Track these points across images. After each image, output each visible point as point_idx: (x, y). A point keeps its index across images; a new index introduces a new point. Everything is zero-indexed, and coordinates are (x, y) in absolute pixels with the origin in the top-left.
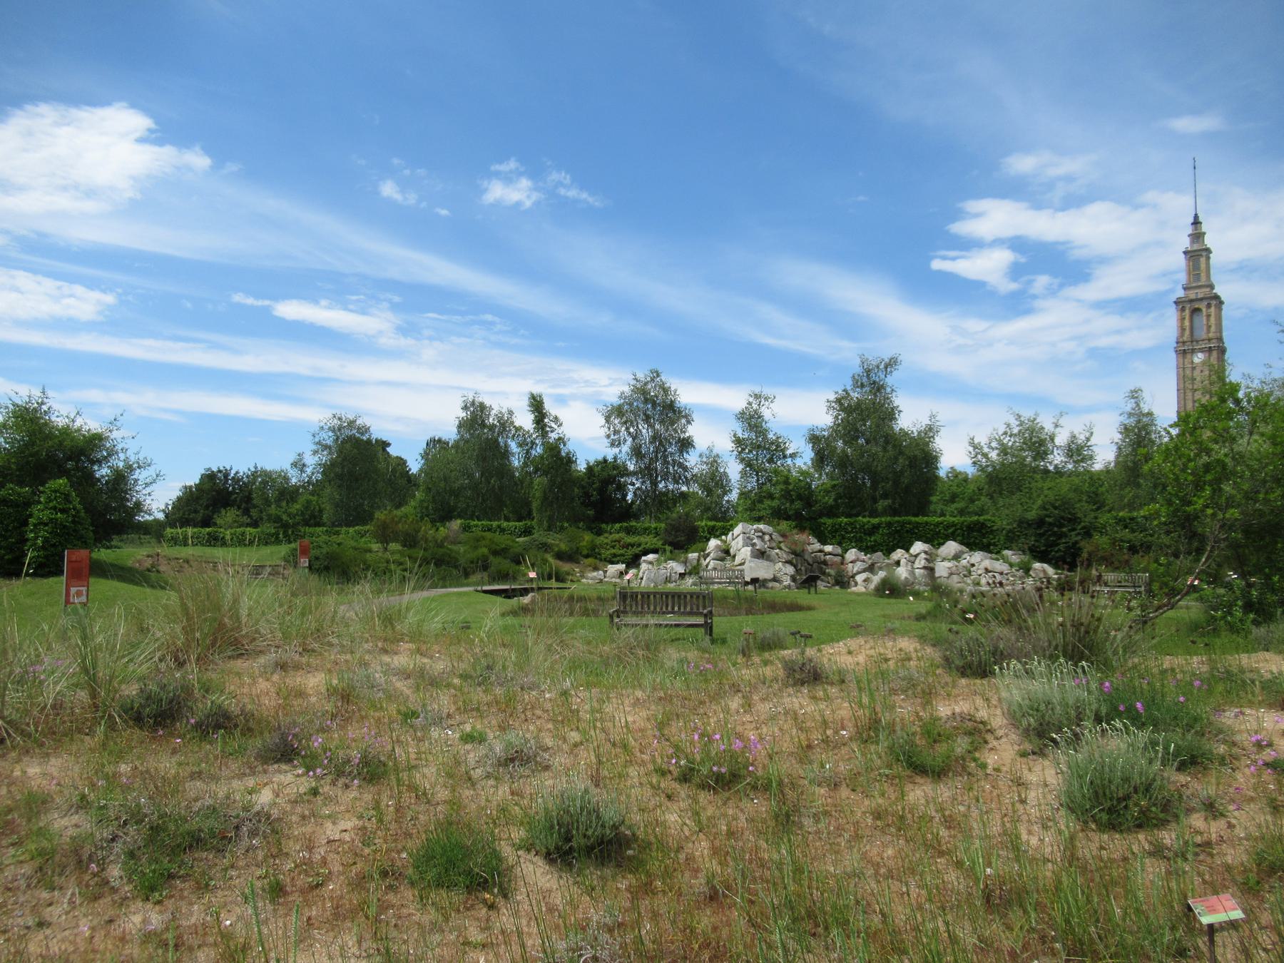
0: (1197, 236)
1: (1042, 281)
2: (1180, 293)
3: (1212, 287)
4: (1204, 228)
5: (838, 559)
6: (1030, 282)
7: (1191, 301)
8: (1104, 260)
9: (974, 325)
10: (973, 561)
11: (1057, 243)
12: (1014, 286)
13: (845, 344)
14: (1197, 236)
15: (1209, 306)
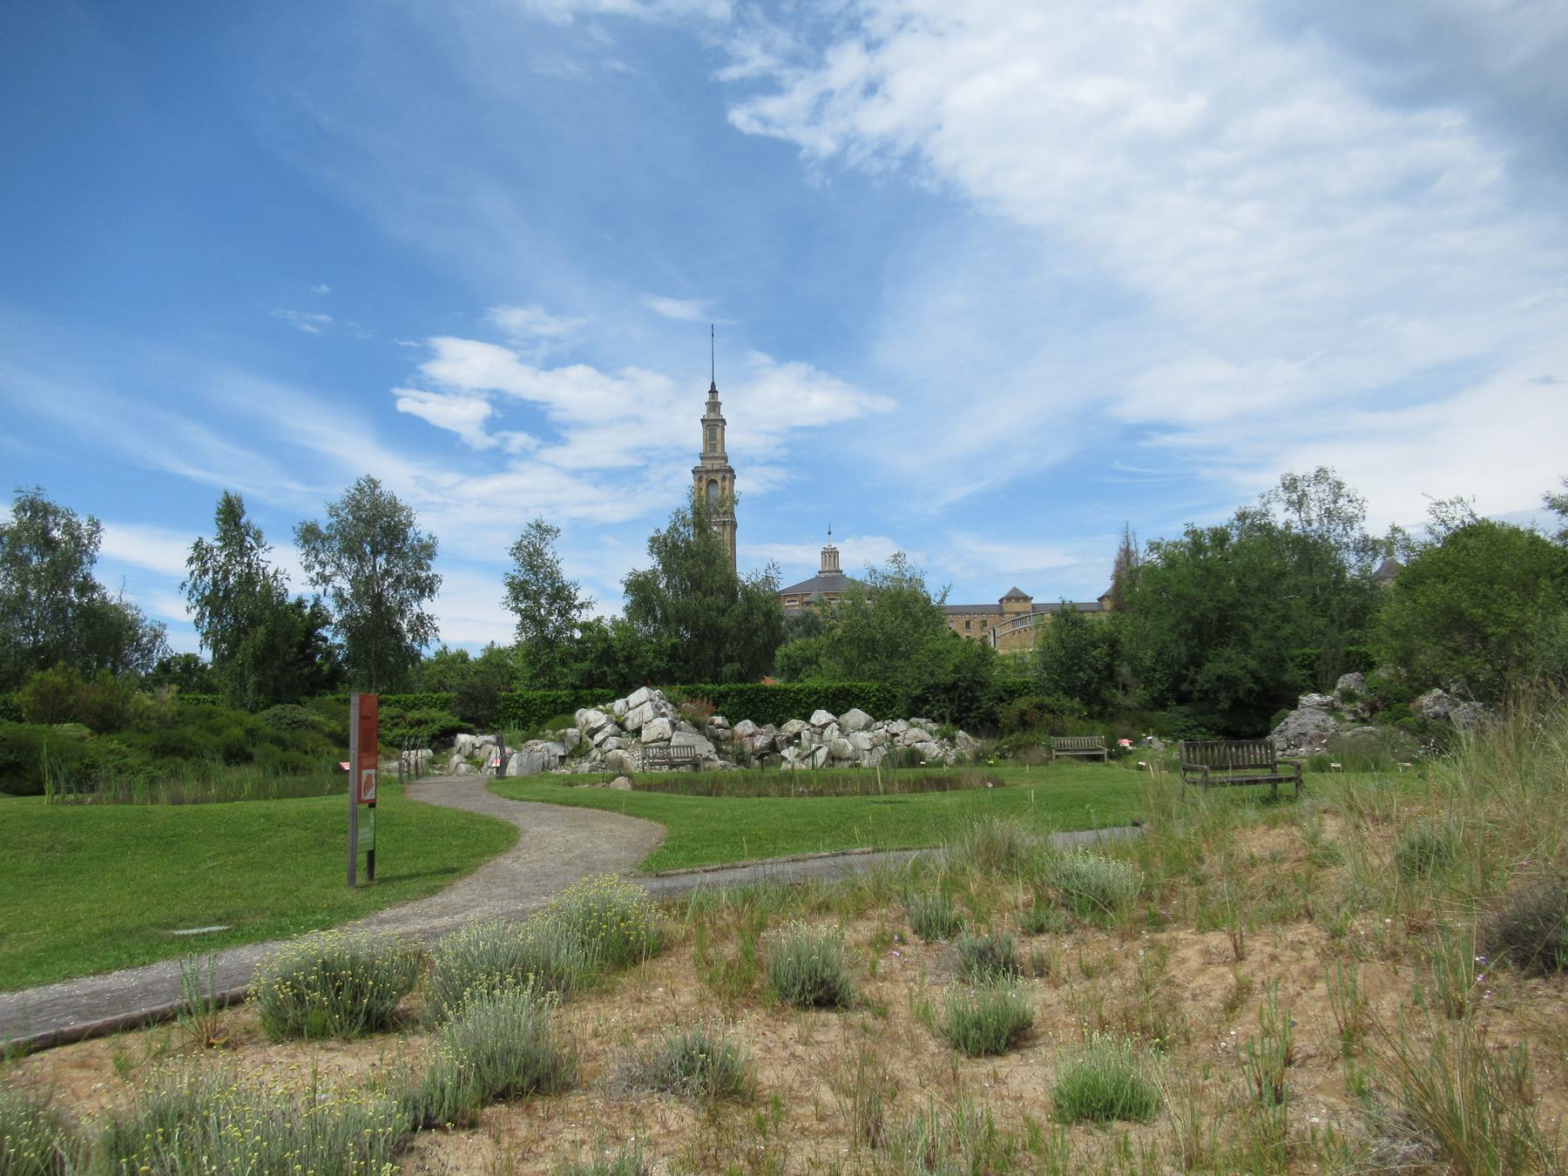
0: (714, 406)
1: (519, 440)
2: (698, 463)
3: (726, 459)
4: (720, 398)
5: (728, 733)
6: (506, 440)
7: (708, 472)
8: (582, 426)
9: (449, 478)
10: (894, 730)
11: (535, 403)
12: (491, 442)
13: (296, 486)
14: (714, 406)
15: (724, 478)
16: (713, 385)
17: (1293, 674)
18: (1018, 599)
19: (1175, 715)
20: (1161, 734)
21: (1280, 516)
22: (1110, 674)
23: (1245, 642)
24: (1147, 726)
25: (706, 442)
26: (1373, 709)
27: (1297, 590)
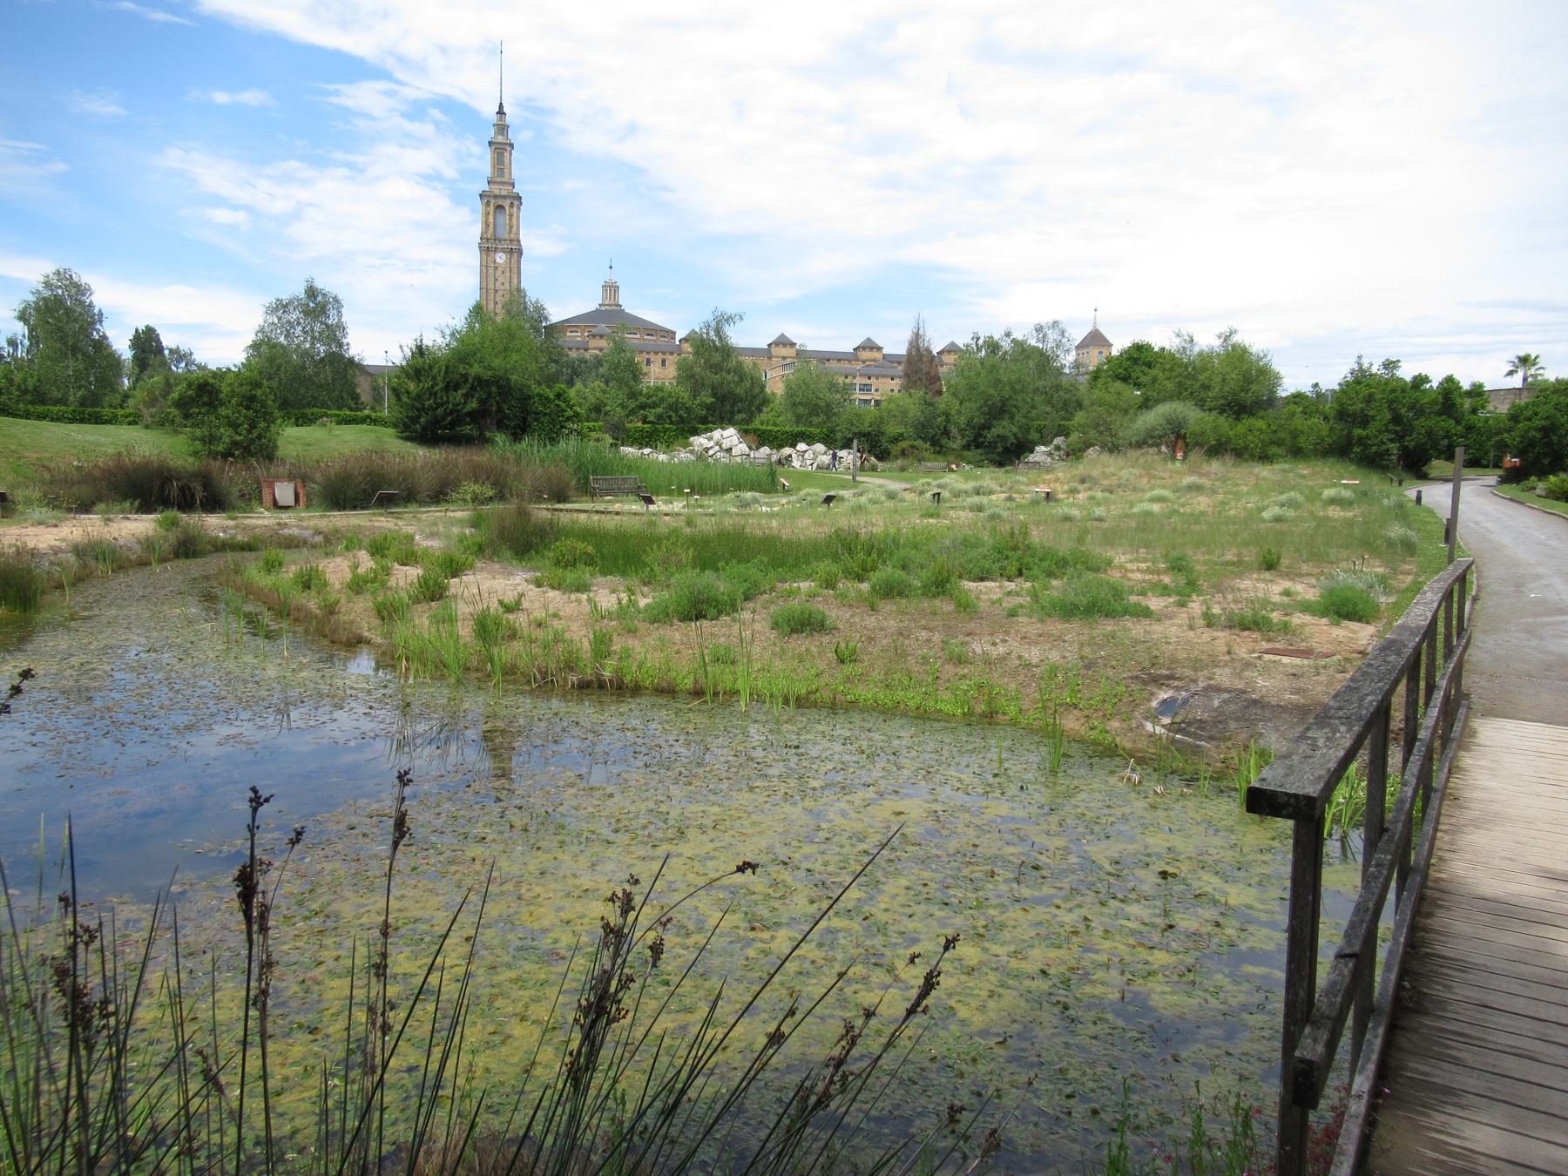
7: (496, 197)
15: (512, 205)
16: (501, 106)
17: (1034, 436)
18: (785, 345)
19: (973, 454)
20: (969, 463)
22: (946, 433)
23: (1012, 418)
24: (963, 459)
25: (493, 166)
26: (1068, 455)
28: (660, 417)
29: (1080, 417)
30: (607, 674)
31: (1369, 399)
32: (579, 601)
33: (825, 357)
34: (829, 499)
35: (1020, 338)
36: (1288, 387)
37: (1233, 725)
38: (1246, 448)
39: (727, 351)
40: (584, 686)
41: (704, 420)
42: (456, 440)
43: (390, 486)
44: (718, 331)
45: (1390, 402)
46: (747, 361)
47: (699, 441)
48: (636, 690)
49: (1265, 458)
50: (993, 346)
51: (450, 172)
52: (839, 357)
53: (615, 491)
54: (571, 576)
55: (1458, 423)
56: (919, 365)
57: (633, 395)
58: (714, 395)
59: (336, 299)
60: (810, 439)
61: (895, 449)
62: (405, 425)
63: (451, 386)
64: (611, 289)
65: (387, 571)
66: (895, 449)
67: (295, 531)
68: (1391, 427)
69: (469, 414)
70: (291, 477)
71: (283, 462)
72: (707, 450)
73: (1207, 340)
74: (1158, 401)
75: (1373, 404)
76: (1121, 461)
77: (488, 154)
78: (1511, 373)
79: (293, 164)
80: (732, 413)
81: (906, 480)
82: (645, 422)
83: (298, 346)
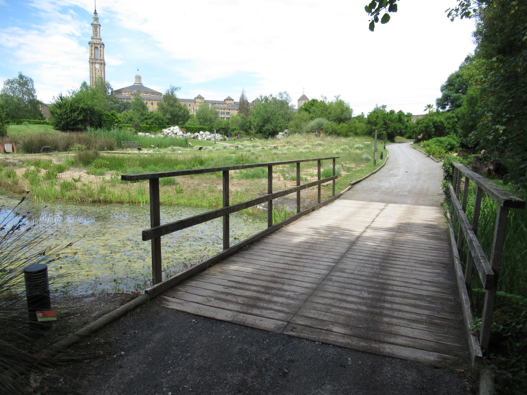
7: (94, 44)
15: (101, 47)
17: (278, 129)
19: (259, 135)
21: (278, 98)
22: (250, 128)
23: (271, 124)
24: (256, 137)
27: (279, 114)
28: (152, 122)
29: (291, 123)
30: (101, 198)
31: (377, 117)
32: (100, 178)
33: (214, 103)
34: (200, 149)
35: (274, 97)
36: (355, 114)
37: (279, 205)
38: (341, 133)
39: (176, 100)
40: (94, 202)
41: (168, 124)
42: (73, 130)
43: (48, 145)
44: (172, 93)
45: (383, 118)
46: (182, 104)
47: (166, 131)
48: (111, 202)
49: (346, 136)
50: (266, 99)
51: (78, 34)
52: (219, 103)
53: (130, 147)
54: (98, 170)
55: (403, 125)
56: (243, 105)
57: (142, 115)
58: (171, 115)
59: (31, 80)
60: (204, 130)
61: (233, 133)
62: (56, 124)
63: (73, 111)
64: (138, 78)
65: (39, 171)
66: (233, 133)
67: (12, 161)
68: (384, 126)
69: (80, 121)
70: (11, 142)
71: (8, 137)
72: (168, 134)
73: (330, 99)
74: (316, 118)
75: (379, 119)
76: (301, 136)
77: (91, 28)
78: (425, 110)
79: (16, 28)
80: (178, 121)
81: (230, 143)
82: (147, 124)
83: (17, 96)
